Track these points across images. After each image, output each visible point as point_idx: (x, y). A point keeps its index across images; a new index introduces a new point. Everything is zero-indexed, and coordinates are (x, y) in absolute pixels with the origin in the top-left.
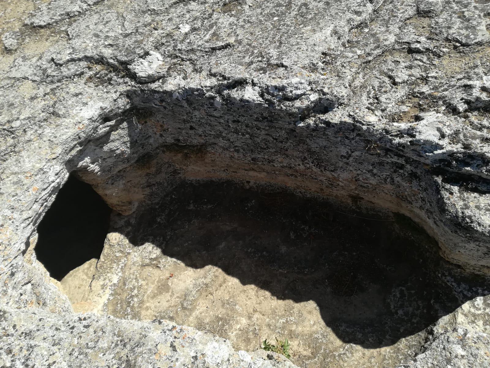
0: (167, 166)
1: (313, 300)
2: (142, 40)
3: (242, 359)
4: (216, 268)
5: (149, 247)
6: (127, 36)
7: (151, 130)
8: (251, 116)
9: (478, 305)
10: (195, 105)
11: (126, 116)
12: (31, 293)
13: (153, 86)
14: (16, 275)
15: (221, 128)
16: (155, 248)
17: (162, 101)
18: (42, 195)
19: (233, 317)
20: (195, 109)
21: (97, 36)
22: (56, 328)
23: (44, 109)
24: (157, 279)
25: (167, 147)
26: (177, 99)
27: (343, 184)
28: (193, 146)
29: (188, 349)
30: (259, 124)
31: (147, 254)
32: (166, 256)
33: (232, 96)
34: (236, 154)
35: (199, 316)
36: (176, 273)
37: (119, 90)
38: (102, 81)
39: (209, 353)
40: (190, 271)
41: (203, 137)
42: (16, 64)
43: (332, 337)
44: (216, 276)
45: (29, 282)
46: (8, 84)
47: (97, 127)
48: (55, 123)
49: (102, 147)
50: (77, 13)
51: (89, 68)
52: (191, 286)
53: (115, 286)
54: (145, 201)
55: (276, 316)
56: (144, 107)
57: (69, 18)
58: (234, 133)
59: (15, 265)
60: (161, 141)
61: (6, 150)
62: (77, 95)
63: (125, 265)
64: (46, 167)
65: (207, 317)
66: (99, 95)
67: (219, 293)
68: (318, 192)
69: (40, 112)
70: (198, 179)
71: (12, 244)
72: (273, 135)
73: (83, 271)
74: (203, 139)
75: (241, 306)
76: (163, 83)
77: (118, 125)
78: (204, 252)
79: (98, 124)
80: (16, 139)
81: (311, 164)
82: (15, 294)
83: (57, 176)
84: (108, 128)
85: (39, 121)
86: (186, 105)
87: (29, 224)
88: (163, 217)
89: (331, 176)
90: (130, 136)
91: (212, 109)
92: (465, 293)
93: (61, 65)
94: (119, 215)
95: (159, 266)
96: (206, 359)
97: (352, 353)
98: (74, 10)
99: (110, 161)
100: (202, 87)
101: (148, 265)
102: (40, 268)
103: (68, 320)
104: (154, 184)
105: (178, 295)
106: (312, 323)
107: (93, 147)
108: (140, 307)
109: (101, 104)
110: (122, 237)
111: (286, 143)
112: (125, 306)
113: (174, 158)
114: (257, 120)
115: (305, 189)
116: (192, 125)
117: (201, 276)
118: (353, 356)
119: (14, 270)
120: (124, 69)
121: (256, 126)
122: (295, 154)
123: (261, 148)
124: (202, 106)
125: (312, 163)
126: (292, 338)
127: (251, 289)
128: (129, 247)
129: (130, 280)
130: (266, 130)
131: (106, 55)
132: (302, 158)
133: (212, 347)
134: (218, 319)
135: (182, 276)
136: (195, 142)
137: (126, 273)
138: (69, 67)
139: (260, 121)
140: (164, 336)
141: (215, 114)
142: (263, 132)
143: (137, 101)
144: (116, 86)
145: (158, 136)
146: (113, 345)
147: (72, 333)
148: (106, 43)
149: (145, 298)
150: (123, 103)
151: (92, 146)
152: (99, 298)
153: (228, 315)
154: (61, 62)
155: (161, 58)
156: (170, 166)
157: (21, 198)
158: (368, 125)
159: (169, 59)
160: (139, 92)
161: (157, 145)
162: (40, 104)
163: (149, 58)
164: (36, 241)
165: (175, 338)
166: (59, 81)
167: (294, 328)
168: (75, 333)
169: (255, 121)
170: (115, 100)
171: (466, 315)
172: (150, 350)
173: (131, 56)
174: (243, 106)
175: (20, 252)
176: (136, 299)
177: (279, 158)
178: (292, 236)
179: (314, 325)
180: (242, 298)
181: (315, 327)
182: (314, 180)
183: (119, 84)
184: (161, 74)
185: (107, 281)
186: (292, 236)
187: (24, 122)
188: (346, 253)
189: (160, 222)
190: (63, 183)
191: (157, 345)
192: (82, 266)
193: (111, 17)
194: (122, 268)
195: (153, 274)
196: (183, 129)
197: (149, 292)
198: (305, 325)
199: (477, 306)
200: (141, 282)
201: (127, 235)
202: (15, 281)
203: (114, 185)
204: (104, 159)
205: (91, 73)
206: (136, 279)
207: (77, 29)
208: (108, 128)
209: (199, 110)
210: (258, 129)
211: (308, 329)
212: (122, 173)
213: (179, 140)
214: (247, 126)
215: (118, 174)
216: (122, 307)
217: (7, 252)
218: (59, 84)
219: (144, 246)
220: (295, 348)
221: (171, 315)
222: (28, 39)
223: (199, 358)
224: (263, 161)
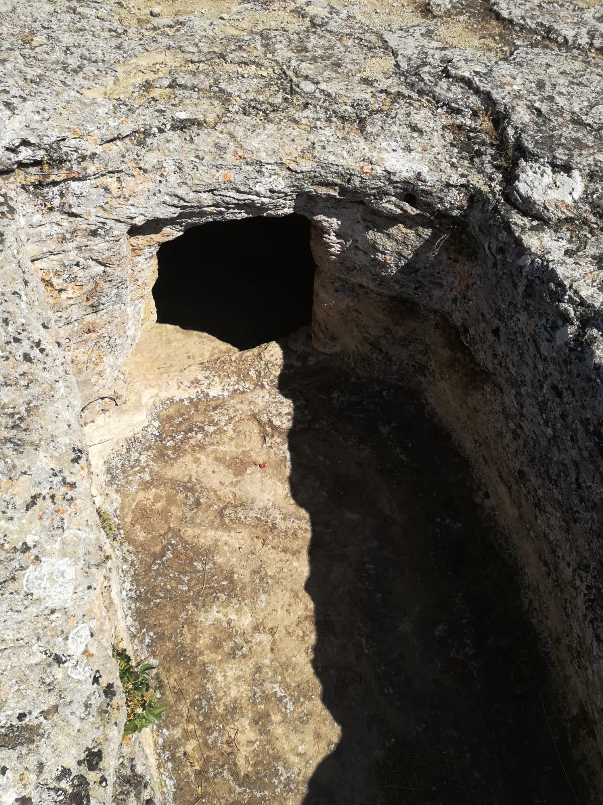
0: (421, 348)
1: (343, 731)
2: (587, 147)
3: (71, 636)
4: (308, 527)
5: (287, 406)
6: (577, 121)
7: (451, 279)
8: (583, 407)
10: (533, 303)
11: (440, 224)
12: (93, 277)
13: (517, 219)
14: (97, 240)
15: (529, 376)
16: (290, 417)
17: (501, 250)
18: (228, 194)
19: (244, 599)
20: (526, 308)
21: (541, 85)
22: (7, 319)
23: (358, 105)
24: (246, 449)
25: (445, 324)
26: (521, 268)
27: (591, 678)
28: (473, 359)
29: (38, 528)
30: (581, 434)
31: (274, 412)
32: (287, 440)
33: (594, 347)
34: (509, 436)
35: (220, 543)
36: (269, 470)
37: (469, 178)
38: (466, 145)
39: (46, 567)
40: (283, 489)
41: (496, 361)
42: (411, 30)
44: (295, 534)
45: (105, 266)
46: (370, 42)
47: (386, 194)
48: (348, 133)
49: (368, 228)
50: (561, 40)
51: (475, 114)
52: (261, 504)
53: (204, 397)
54: (349, 357)
55: (281, 674)
56: (474, 233)
57: (543, 37)
58: (538, 403)
59: (108, 228)
60: (448, 306)
61: (261, 103)
62: (414, 128)
63: (243, 392)
64: (269, 167)
65: (225, 555)
66: (439, 156)
67: (273, 555)
68: (550, 635)
69: (349, 102)
70: (438, 410)
71: (130, 202)
72: (583, 475)
73: (214, 348)
74: (493, 364)
75: (268, 603)
76: (532, 228)
77: (418, 224)
78: (325, 494)
79: (392, 191)
80: (286, 105)
81: (583, 587)
82: (73, 255)
83: (269, 194)
84: (399, 211)
85: (334, 112)
86: (521, 289)
87: (174, 206)
88: (342, 398)
89: (588, 642)
90: (416, 253)
91: (547, 335)
93: (448, 76)
94: (309, 337)
95: (267, 439)
96: (31, 567)
98: (564, 32)
99: (361, 259)
100: (571, 287)
101: (259, 422)
102: (148, 271)
103: (29, 328)
104: (381, 351)
105: (238, 493)
106: (301, 749)
107: (358, 215)
108: (193, 450)
109: (425, 170)
110: (280, 362)
111: (587, 510)
112: (183, 427)
113: (438, 350)
114: (585, 423)
115: (540, 606)
116: (501, 328)
117: (284, 511)
120: (511, 156)
121: (575, 431)
122: (581, 542)
123: (547, 472)
124: (540, 315)
125: (588, 587)
126: (257, 723)
127: (306, 605)
128: (272, 381)
129: (226, 412)
130: (582, 456)
131: (514, 117)
132: (585, 562)
133: (62, 568)
134: (230, 578)
135: (270, 482)
136: (481, 357)
137: (232, 401)
138: (453, 88)
139: (587, 431)
140: (47, 476)
141: (544, 347)
142: (574, 453)
143: (476, 216)
144: (473, 171)
145: (450, 296)
146: (10, 411)
147: (8, 343)
148: (537, 105)
149: (211, 448)
150: (455, 198)
151: (357, 213)
152: (176, 386)
153: (243, 589)
154: (453, 72)
155: (577, 195)
156: (425, 353)
157: (201, 168)
159: (587, 207)
160: (490, 208)
161: (437, 307)
162: (363, 94)
163: (562, 177)
164: (171, 238)
165: (53, 497)
166: (420, 93)
167: (276, 718)
168: (8, 348)
169: (582, 422)
170: (448, 185)
172: (14, 467)
173: (543, 149)
174: (589, 379)
175: (130, 221)
176: (200, 436)
177: (555, 518)
178: (439, 630)
179: (299, 754)
180: (282, 597)
181: (296, 759)
182: (564, 614)
183: (481, 171)
184: (547, 215)
185: (206, 382)
186: (439, 630)
187: (318, 94)
188: (468, 756)
189: (332, 398)
190: (272, 212)
191: (25, 473)
192: (221, 342)
193: (595, 84)
194: (235, 391)
195: (251, 437)
196: (485, 321)
197: (222, 448)
198: (291, 737)
200: (229, 429)
201: (286, 367)
202: (89, 243)
203: (336, 294)
204: (357, 247)
205: (469, 122)
206: (231, 418)
207: (530, 57)
208: (399, 211)
209: (531, 317)
210: (572, 440)
211: (286, 747)
212: (361, 292)
213: (466, 331)
214: (563, 416)
215: (357, 288)
216: (181, 423)
217: (115, 203)
218: (415, 96)
219: (284, 400)
220: (242, 738)
221: (201, 501)
222: (466, 18)
223: (27, 554)
224: (529, 492)
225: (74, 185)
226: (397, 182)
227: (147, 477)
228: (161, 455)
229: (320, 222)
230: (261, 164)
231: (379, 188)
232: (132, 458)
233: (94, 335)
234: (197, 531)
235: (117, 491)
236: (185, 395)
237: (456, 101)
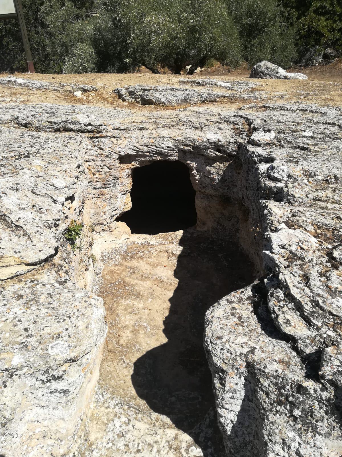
9: (192, 451)
14: (108, 159)
43: (138, 355)
44: (171, 284)
49: (207, 166)
51: (243, 124)
82: (100, 163)
92: (202, 434)
94: (196, 228)
97: (126, 367)
109: (221, 139)
110: (182, 235)
118: (123, 368)
119: (109, 156)
158: (269, 211)
170: (230, 142)
171: (176, 438)
179: (148, 344)
199: (190, 450)
225: (103, 139)
226: (211, 143)
227: (117, 263)
228: (125, 258)
229: (189, 164)
230: (164, 137)
231: (205, 146)
232: (113, 256)
233: (104, 197)
234: (131, 280)
235: (104, 264)
236: (140, 242)
237: (236, 121)
